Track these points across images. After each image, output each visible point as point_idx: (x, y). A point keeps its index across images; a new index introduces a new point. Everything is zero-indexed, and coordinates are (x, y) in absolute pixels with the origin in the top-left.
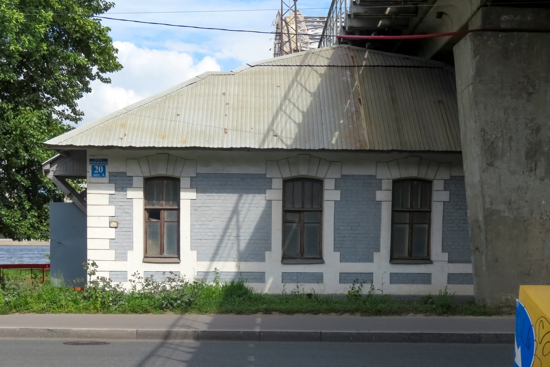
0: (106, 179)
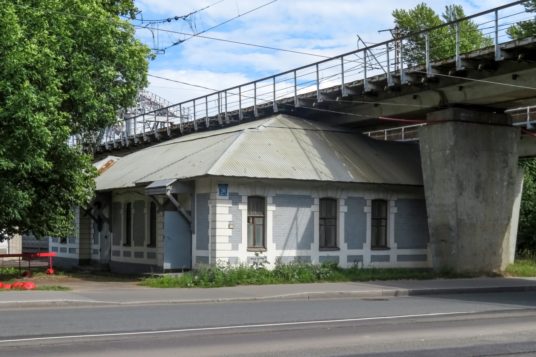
0: (227, 198)
